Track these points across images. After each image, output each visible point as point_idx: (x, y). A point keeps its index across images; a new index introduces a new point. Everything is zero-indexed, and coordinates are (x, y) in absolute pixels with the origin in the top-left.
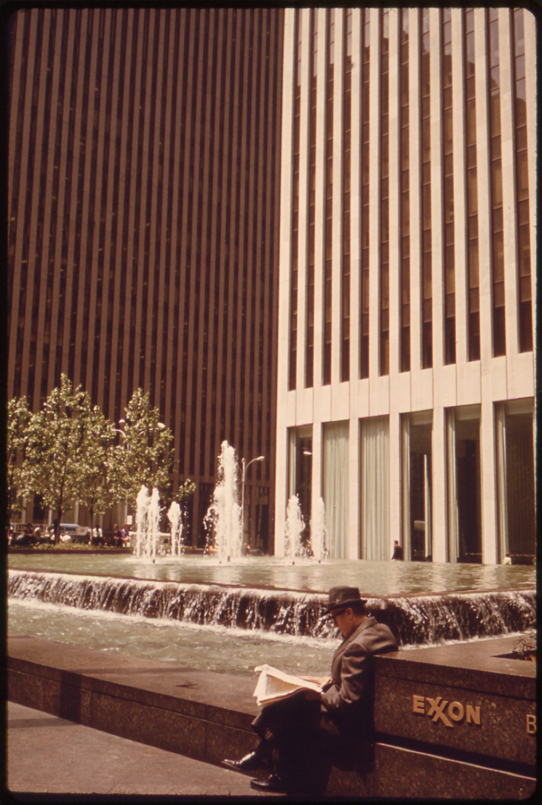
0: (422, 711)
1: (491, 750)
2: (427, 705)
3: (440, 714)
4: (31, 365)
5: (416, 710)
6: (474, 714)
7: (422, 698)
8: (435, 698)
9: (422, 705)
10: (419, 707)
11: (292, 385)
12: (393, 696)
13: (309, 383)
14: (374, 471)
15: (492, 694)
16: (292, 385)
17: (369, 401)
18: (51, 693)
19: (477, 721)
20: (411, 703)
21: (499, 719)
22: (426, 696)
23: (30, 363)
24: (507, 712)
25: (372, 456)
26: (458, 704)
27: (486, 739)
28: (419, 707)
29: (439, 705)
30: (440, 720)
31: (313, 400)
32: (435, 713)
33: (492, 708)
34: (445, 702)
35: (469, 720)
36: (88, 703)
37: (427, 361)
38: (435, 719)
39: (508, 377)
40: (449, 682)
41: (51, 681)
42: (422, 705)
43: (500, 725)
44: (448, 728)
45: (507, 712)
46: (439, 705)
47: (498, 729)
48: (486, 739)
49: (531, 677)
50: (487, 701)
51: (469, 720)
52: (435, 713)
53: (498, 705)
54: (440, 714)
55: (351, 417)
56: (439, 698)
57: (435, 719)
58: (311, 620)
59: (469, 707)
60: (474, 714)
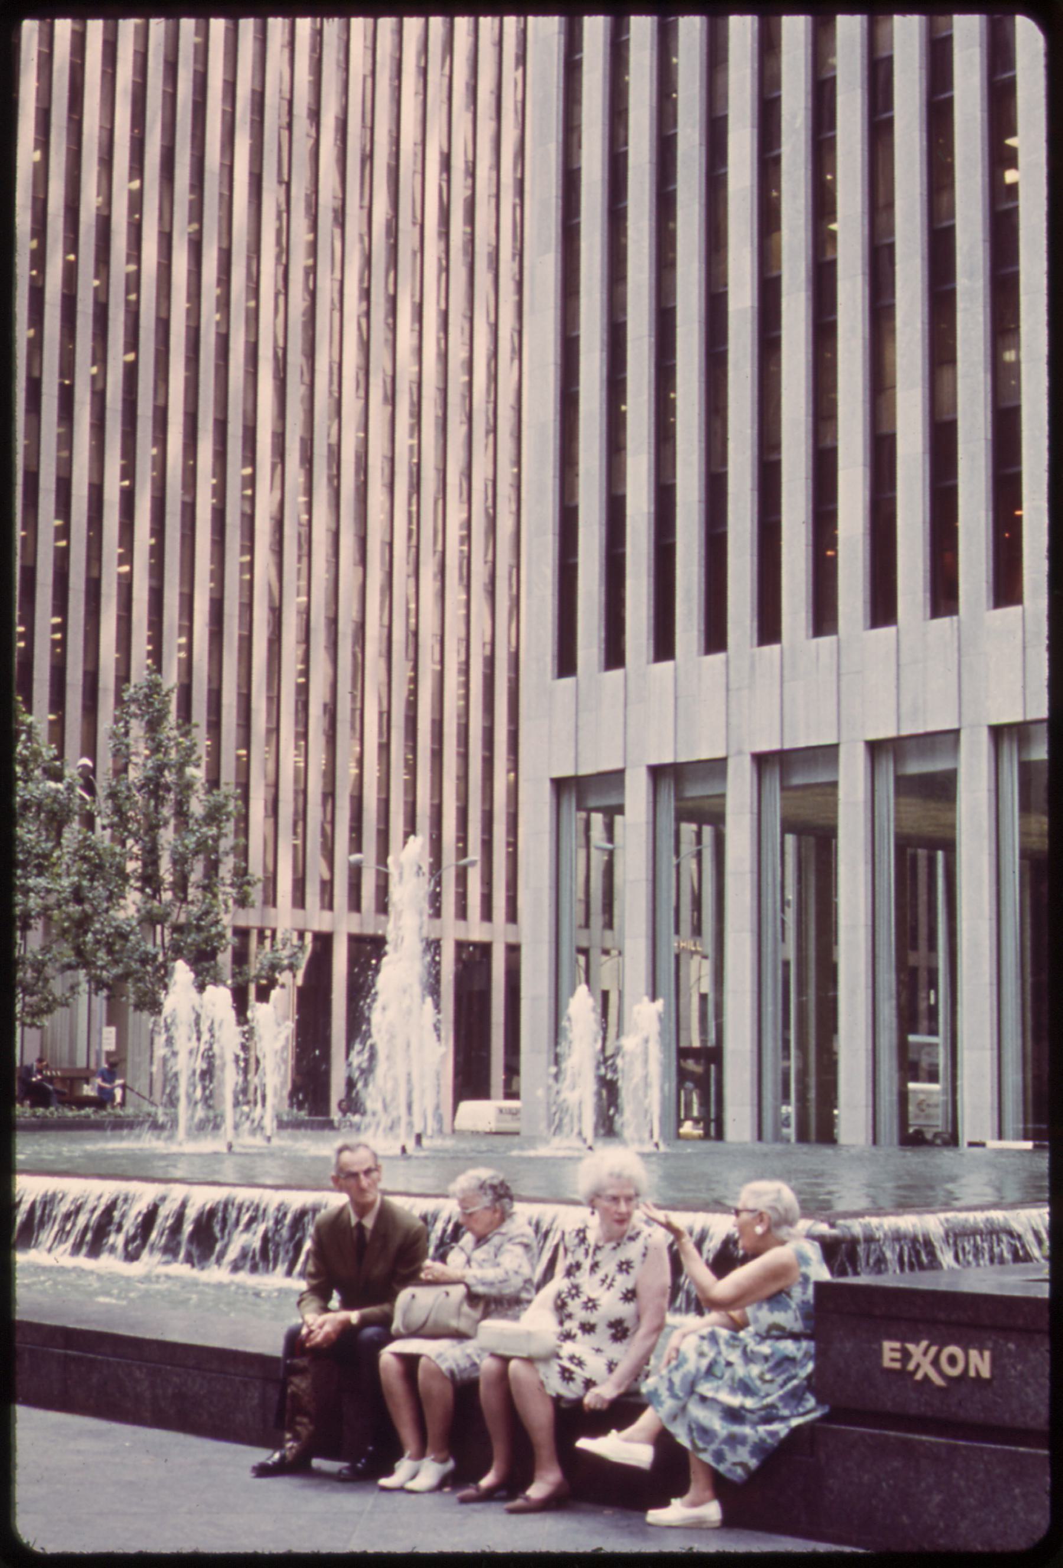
0: (897, 1365)
1: (1007, 1416)
2: (906, 1356)
3: (927, 1369)
4: (126, 483)
5: (887, 1363)
6: (980, 1363)
7: (897, 1345)
8: (917, 1342)
9: (898, 1355)
10: (893, 1360)
11: (566, 665)
12: (848, 1346)
13: (769, 629)
14: (672, 913)
15: (1006, 1330)
16: (566, 665)
17: (625, 733)
18: (170, 1391)
19: (986, 1373)
20: (879, 1353)
21: (1019, 1367)
22: (903, 1340)
23: (123, 477)
24: (1032, 1356)
25: (770, 862)
26: (953, 1349)
27: (1000, 1400)
28: (893, 1360)
29: (925, 1353)
30: (926, 1377)
31: (626, 705)
32: (918, 1366)
33: (1009, 1350)
34: (934, 1350)
35: (972, 1373)
36: (256, 1402)
37: (824, 618)
38: (919, 1376)
39: (970, 673)
40: (942, 1316)
41: (169, 1367)
42: (898, 1355)
43: (1021, 1375)
44: (940, 1389)
45: (1032, 1356)
46: (925, 1353)
47: (1017, 1382)
48: (1000, 1400)
49: (1040, 1296)
50: (1001, 1341)
51: (972, 1373)
52: (918, 1366)
53: (1018, 1346)
54: (927, 1369)
55: (964, 723)
56: (924, 1344)
57: (919, 1376)
58: (957, 1204)
59: (974, 1353)
60: (980, 1363)
